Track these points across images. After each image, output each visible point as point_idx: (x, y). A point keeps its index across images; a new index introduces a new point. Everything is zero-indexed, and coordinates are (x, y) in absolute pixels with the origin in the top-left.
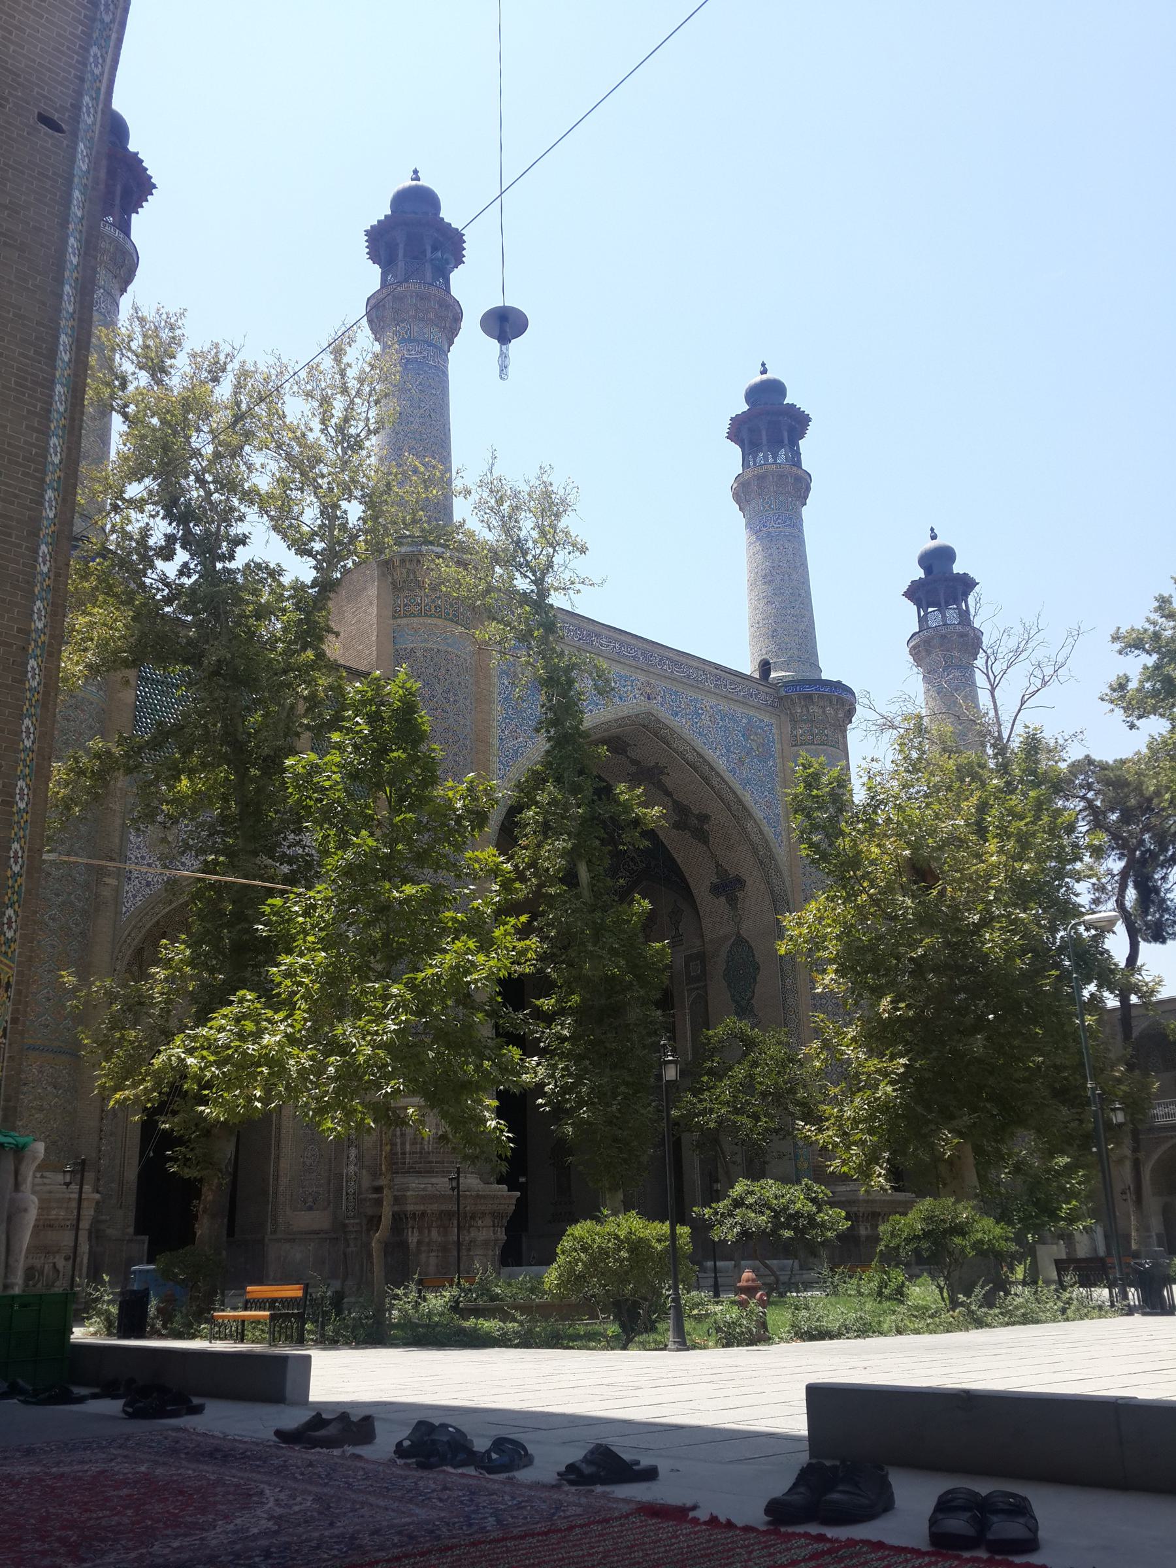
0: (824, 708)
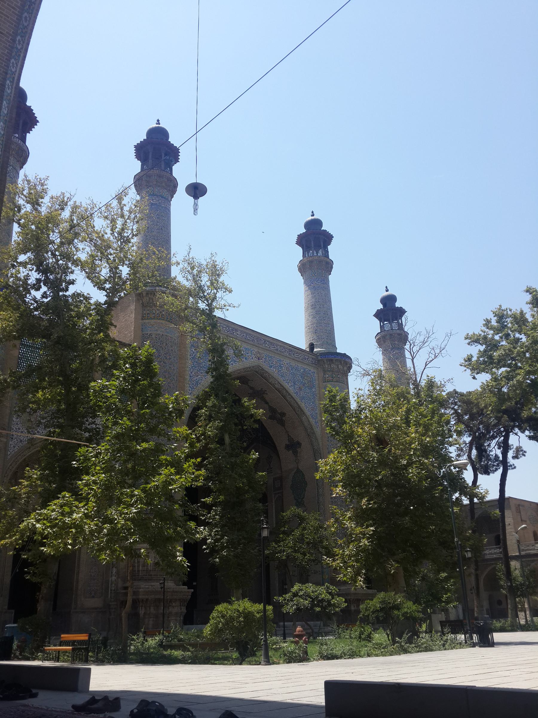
0: (338, 365)
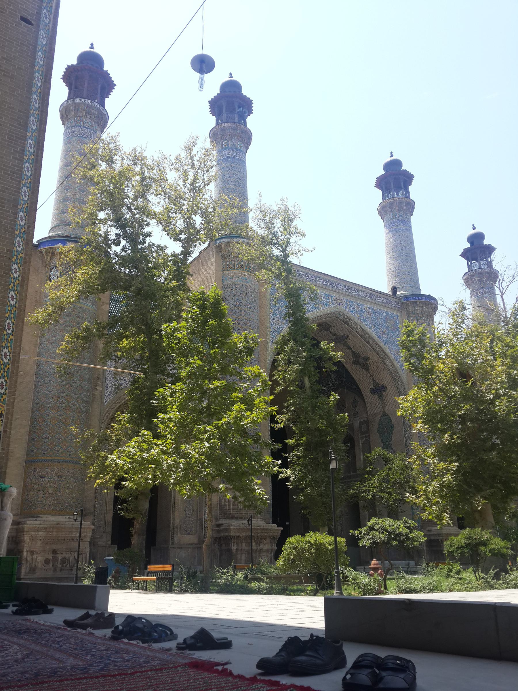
0: (422, 307)
